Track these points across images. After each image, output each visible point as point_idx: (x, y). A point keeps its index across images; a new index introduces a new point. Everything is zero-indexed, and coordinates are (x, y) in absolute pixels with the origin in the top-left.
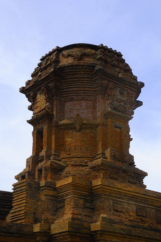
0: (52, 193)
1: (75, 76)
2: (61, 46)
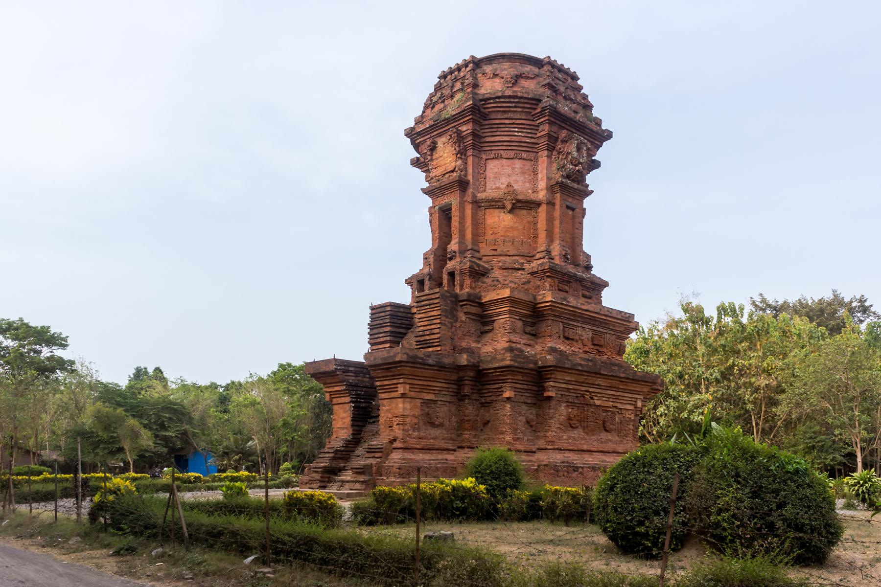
0: (473, 310)
1: (506, 116)
2: (479, 56)
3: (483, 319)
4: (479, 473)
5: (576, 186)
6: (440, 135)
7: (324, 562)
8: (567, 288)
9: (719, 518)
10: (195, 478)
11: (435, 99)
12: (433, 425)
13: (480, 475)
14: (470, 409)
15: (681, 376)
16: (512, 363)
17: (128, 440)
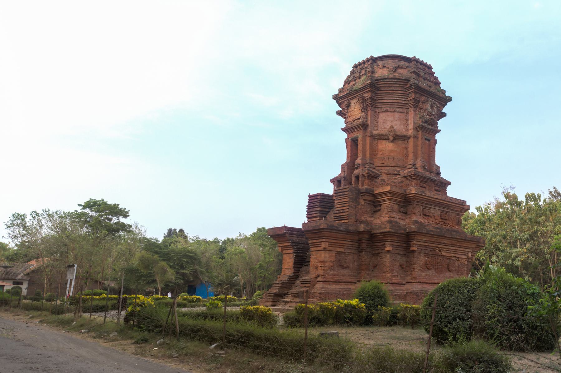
1: (390, 89)
2: (376, 56)
3: (375, 204)
4: (362, 297)
5: (430, 127)
6: (353, 99)
7: (256, 347)
8: (425, 185)
9: (489, 322)
10: (197, 299)
11: (350, 79)
12: (343, 267)
13: (363, 298)
14: (366, 257)
15: (505, 237)
16: (390, 230)
17: (160, 275)
